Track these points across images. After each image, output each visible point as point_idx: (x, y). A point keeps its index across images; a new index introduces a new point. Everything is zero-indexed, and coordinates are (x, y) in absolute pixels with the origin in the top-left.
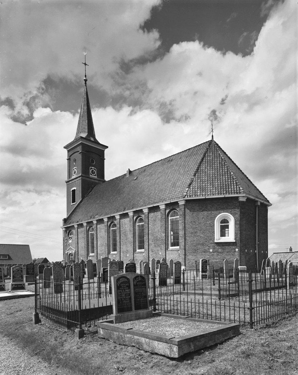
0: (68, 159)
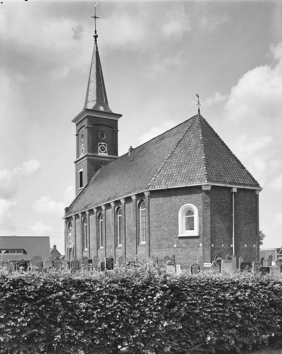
0: (76, 135)
